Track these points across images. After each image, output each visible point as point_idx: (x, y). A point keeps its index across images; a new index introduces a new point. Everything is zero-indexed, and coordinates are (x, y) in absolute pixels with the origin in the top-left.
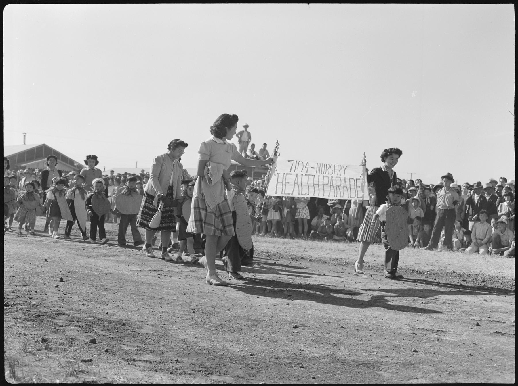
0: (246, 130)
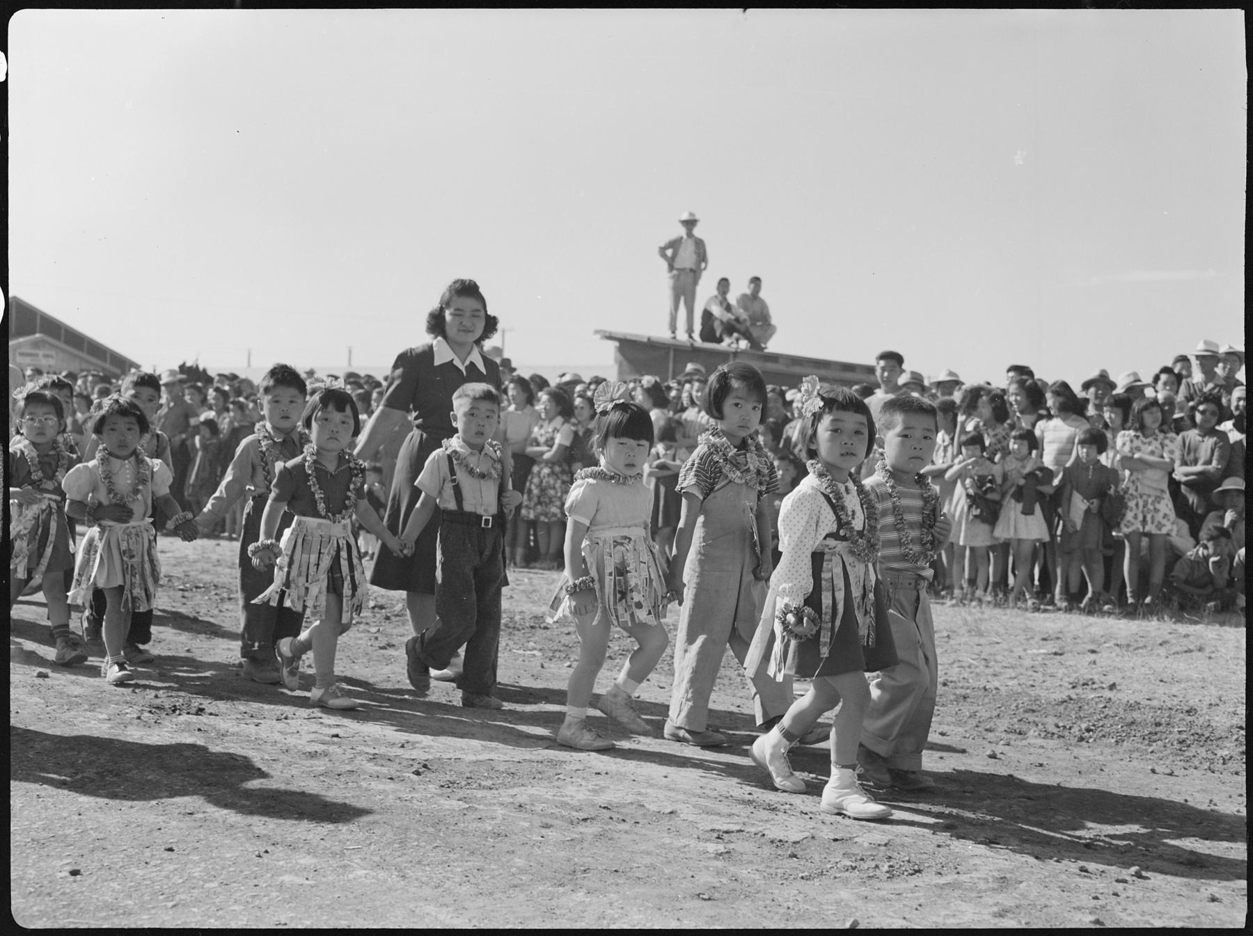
0: (690, 235)
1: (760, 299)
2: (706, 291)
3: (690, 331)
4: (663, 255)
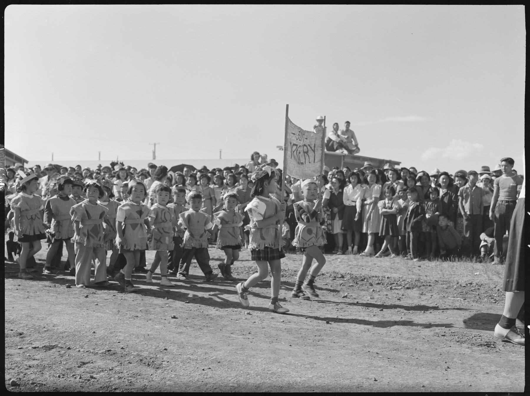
1: (351, 131)
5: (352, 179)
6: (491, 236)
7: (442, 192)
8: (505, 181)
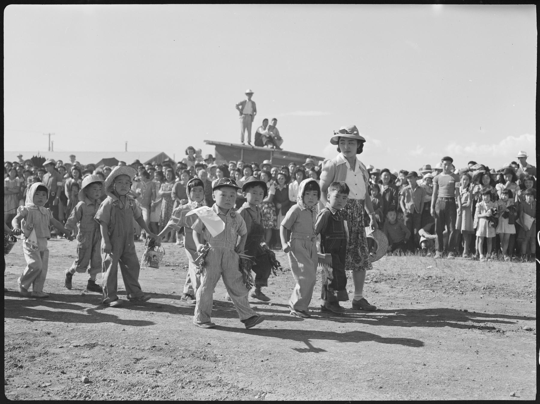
0: (250, 99)
2: (257, 125)
3: (249, 142)
4: (238, 108)
5: (298, 175)
6: (431, 232)
7: (383, 188)
8: (444, 178)
